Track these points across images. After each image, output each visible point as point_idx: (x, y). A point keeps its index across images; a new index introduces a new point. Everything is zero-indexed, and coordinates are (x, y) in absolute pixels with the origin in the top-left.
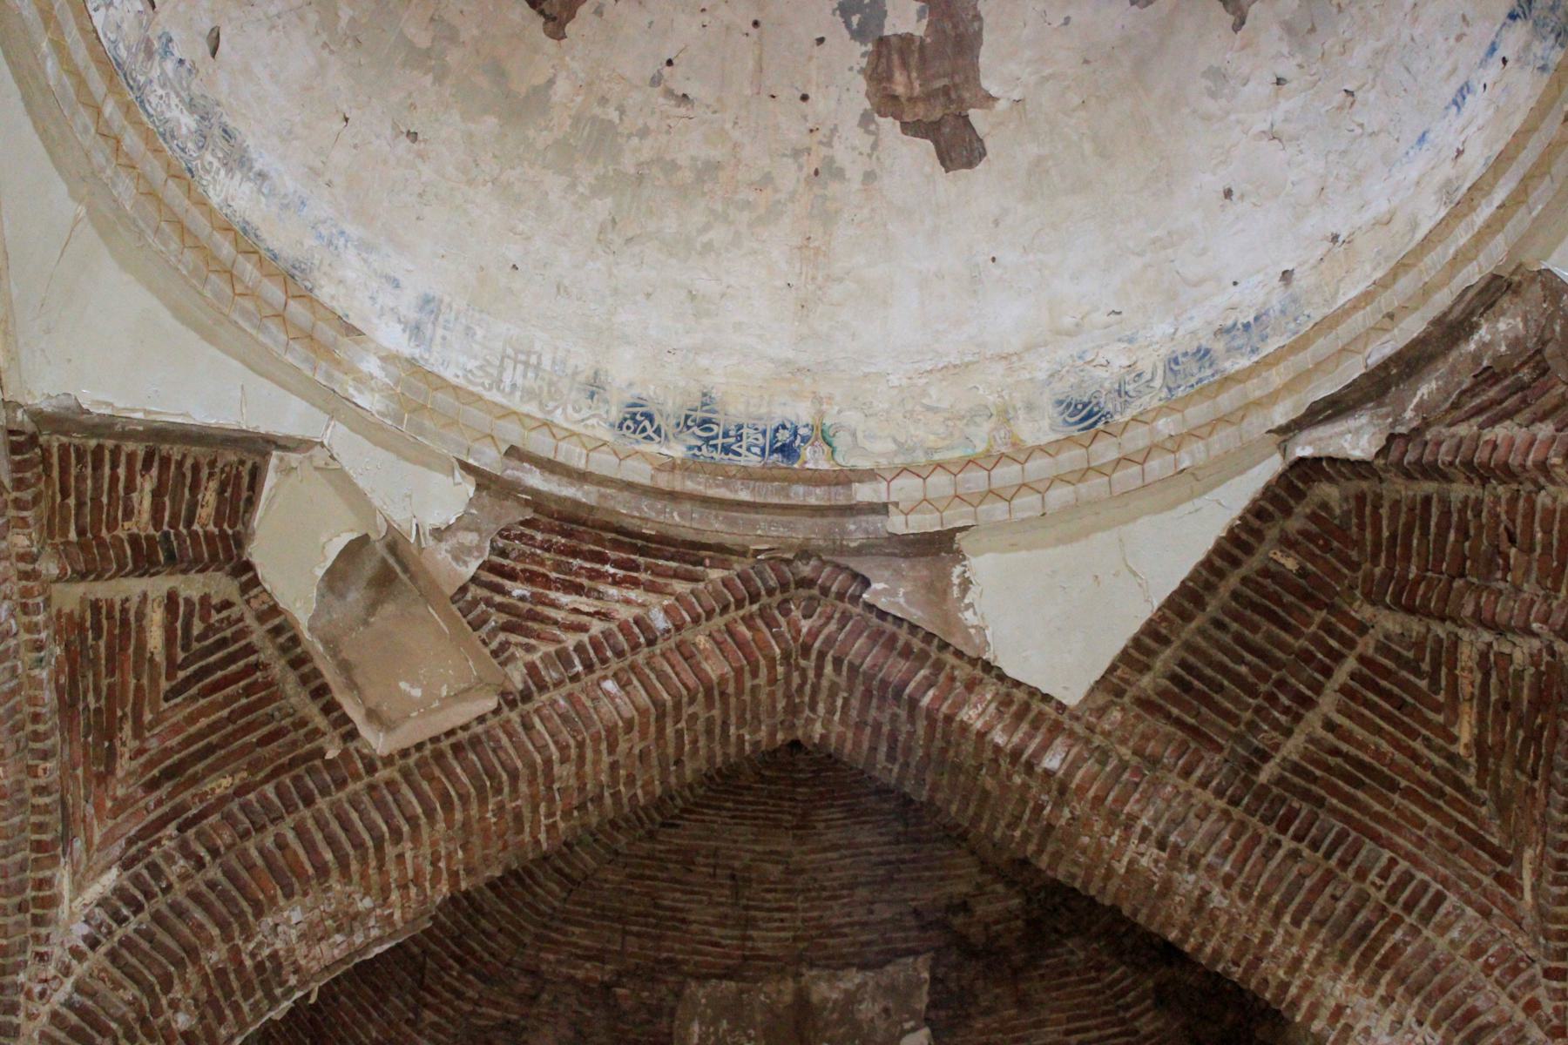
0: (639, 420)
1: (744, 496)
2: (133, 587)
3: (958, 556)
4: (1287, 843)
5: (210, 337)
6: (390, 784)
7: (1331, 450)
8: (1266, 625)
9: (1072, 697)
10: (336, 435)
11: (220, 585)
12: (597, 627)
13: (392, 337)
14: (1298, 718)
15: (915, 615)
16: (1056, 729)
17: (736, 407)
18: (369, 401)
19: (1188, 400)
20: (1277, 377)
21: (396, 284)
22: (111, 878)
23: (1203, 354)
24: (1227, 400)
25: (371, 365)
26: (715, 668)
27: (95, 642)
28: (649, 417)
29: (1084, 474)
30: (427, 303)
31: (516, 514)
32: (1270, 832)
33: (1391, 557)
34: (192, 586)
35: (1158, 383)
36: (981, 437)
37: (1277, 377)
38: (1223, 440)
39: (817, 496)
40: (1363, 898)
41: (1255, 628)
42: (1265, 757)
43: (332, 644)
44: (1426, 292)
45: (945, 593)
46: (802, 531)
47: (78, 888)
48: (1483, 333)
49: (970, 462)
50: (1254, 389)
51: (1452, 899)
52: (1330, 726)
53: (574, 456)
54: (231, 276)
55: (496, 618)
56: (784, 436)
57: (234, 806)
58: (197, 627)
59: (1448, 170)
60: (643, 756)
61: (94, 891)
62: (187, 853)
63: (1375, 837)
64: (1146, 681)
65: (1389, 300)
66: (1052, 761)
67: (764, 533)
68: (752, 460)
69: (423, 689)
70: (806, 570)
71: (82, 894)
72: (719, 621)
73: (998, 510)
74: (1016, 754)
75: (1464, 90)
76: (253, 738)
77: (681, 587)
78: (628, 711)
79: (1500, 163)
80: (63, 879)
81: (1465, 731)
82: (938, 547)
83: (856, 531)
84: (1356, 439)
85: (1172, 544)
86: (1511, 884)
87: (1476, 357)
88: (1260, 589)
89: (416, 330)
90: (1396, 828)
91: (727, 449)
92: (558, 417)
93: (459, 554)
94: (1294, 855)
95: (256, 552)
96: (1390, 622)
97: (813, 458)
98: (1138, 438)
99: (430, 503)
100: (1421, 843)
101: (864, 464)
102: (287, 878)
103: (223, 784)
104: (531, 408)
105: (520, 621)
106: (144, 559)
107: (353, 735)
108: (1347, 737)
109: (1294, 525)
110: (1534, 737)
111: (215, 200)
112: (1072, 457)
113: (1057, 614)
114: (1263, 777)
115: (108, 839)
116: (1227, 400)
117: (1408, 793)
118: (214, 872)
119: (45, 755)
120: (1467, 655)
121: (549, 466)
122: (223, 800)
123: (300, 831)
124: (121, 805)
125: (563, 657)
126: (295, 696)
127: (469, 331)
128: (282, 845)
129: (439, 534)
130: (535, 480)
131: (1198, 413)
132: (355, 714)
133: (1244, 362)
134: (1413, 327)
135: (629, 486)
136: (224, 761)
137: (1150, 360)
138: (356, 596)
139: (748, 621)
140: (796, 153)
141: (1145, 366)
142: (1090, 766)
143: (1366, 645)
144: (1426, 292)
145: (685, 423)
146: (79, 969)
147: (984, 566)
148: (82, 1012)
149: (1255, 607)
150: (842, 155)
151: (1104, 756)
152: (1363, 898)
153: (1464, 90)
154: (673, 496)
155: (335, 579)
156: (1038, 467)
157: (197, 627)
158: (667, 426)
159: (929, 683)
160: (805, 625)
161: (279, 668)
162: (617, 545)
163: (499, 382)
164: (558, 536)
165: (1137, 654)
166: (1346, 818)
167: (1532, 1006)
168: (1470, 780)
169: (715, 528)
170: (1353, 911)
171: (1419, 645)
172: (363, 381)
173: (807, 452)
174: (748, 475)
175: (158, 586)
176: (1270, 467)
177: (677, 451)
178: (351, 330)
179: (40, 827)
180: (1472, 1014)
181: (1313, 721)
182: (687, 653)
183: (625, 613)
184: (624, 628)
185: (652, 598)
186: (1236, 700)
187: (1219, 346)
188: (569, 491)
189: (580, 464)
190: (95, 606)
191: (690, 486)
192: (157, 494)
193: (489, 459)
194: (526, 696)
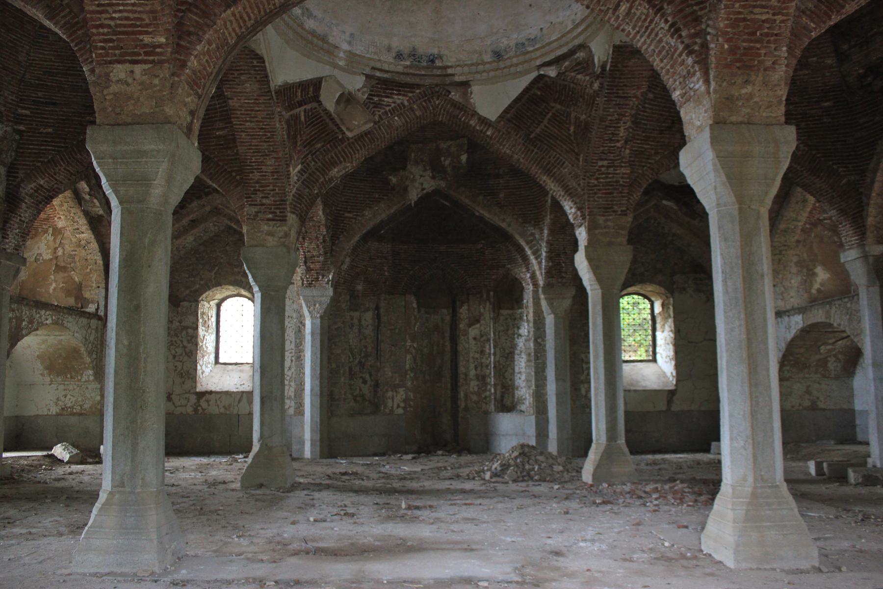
0: (399, 56)
1: (423, 73)
3: (470, 86)
4: (536, 151)
5: (308, 57)
6: (353, 143)
7: (547, 74)
9: (493, 119)
10: (337, 73)
11: (314, 105)
12: (393, 105)
13: (345, 46)
15: (461, 100)
16: (490, 125)
18: (341, 63)
19: (519, 55)
20: (538, 54)
21: (344, 32)
22: (299, 167)
23: (523, 44)
24: (527, 57)
25: (341, 55)
26: (418, 113)
27: (293, 124)
29: (497, 70)
30: (352, 35)
31: (374, 82)
32: (532, 148)
34: (308, 107)
36: (475, 58)
37: (538, 54)
38: (526, 66)
39: (439, 72)
40: (549, 162)
42: (532, 132)
43: (338, 116)
44: (567, 43)
46: (437, 81)
48: (578, 55)
49: (472, 65)
50: (533, 55)
51: (567, 163)
52: (545, 126)
53: (386, 67)
54: (312, 43)
55: (371, 106)
56: (431, 57)
59: (573, 17)
61: (296, 170)
62: (315, 161)
64: (509, 115)
65: (562, 42)
66: (489, 133)
67: (428, 81)
68: (425, 64)
69: (357, 124)
70: (437, 89)
71: (295, 171)
72: (419, 102)
73: (478, 76)
74: (481, 131)
77: (410, 95)
78: (400, 124)
79: (583, 20)
80: (291, 169)
82: (466, 85)
83: (448, 80)
84: (552, 72)
85: (517, 87)
86: (578, 160)
87: (576, 59)
89: (350, 43)
92: (382, 58)
93: (363, 94)
94: (536, 153)
95: (322, 98)
96: (559, 107)
97: (438, 63)
98: (508, 63)
99: (356, 83)
101: (450, 64)
102: (334, 164)
103: (319, 145)
104: (376, 57)
105: (377, 105)
107: (344, 133)
109: (540, 85)
111: (307, 27)
112: (494, 65)
113: (490, 101)
114: (532, 136)
115: (298, 159)
116: (527, 57)
118: (320, 164)
120: (573, 115)
121: (381, 70)
123: (336, 154)
124: (300, 150)
125: (386, 113)
127: (361, 40)
128: (332, 157)
129: (359, 90)
130: (378, 74)
131: (521, 59)
132: (344, 129)
133: (531, 49)
134: (565, 50)
135: (398, 73)
137: (512, 43)
138: (342, 105)
139: (425, 101)
141: (511, 44)
142: (496, 134)
144: (567, 43)
145: (409, 56)
146: (297, 186)
147: (475, 89)
148: (299, 195)
151: (499, 131)
152: (549, 162)
154: (408, 74)
155: (338, 102)
156: (487, 66)
158: (406, 56)
159: (463, 115)
160: (437, 102)
161: (327, 120)
162: (396, 86)
164: (383, 84)
165: (507, 111)
167: (579, 185)
168: (572, 138)
169: (417, 81)
170: (547, 164)
172: (340, 58)
173: (437, 61)
174: (424, 68)
175: (302, 108)
176: (534, 75)
177: (408, 63)
178: (337, 47)
181: (542, 125)
182: (412, 109)
183: (398, 102)
187: (526, 43)
188: (386, 76)
189: (387, 69)
191: (411, 71)
193: (368, 71)
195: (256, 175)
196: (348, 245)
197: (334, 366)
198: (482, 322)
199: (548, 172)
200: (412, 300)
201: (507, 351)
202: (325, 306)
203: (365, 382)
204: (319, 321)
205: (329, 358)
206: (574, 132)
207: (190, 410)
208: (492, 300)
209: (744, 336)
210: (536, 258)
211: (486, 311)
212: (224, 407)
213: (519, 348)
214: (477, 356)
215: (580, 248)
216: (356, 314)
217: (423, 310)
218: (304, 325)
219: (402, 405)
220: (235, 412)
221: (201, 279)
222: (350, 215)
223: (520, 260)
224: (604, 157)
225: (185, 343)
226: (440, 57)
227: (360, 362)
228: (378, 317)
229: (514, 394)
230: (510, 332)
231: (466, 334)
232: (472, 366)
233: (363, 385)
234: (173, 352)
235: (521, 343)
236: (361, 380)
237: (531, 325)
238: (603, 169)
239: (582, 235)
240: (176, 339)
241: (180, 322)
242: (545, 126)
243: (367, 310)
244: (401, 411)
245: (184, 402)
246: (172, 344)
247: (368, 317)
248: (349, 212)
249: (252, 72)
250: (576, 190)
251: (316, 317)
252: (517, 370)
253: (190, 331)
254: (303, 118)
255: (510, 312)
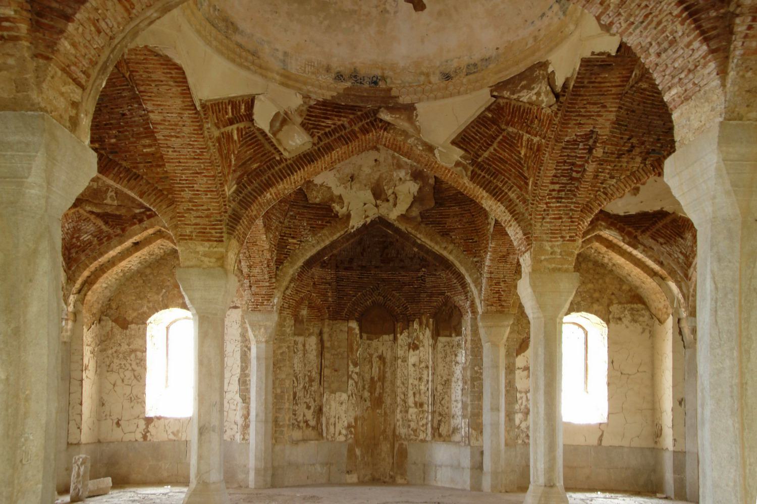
0: (339, 77)
2: (229, 128)
6: (291, 165)
8: (483, 128)
12: (333, 126)
14: (488, 148)
17: (363, 72)
28: (342, 76)
33: (512, 117)
34: (241, 125)
35: (464, 71)
41: (481, 129)
42: (480, 156)
45: (412, 118)
47: (229, 190)
52: (495, 150)
56: (375, 79)
57: (258, 170)
58: (244, 133)
60: (345, 153)
63: (501, 173)
75: (543, 15)
76: (260, 155)
77: (351, 116)
81: (523, 153)
86: (527, 184)
88: (483, 120)
90: (505, 171)
91: (361, 83)
95: (255, 117)
97: (382, 85)
100: (510, 175)
106: (231, 122)
107: (282, 154)
108: (498, 153)
110: (536, 156)
117: (509, 164)
119: (219, 166)
120: (525, 138)
122: (256, 169)
125: (325, 133)
126: (268, 146)
136: (255, 160)
140: (377, 7)
143: (505, 133)
145: (351, 77)
149: (482, 124)
150: (388, 7)
153: (543, 15)
157: (244, 133)
163: (305, 72)
166: (495, 169)
168: (522, 162)
171: (516, 134)
173: (380, 83)
175: (235, 126)
179: (220, 180)
180: (515, 211)
181: (491, 149)
183: (339, 123)
184: (339, 126)
185: (345, 119)
186: (475, 144)
190: (222, 133)
192: (232, 109)
194: (318, 143)
195: (187, 194)
196: (291, 270)
197: (279, 391)
198: (421, 349)
199: (497, 194)
200: (354, 325)
201: (445, 378)
202: (269, 331)
203: (308, 407)
204: (263, 345)
205: (274, 383)
206: (525, 155)
207: (139, 436)
208: (431, 327)
209: (736, 381)
210: (476, 286)
211: (426, 336)
212: (173, 433)
213: (455, 375)
214: (416, 382)
215: (523, 275)
216: (300, 339)
217: (365, 336)
218: (249, 349)
219: (344, 432)
220: (184, 439)
221: (149, 302)
222: (295, 241)
223: (459, 287)
224: (556, 180)
225: (134, 366)
226: (384, 78)
227: (304, 387)
228: (322, 341)
229: (449, 423)
230: (448, 359)
231: (405, 360)
232: (411, 393)
233: (306, 411)
234: (122, 376)
235: (458, 371)
236: (305, 405)
237: (468, 352)
238: (554, 193)
239: (526, 261)
240: (125, 362)
241: (129, 345)
242: (495, 150)
243: (310, 335)
244: (342, 438)
245: (133, 428)
246: (121, 368)
247: (313, 341)
248: (293, 238)
249: (172, 83)
250: (523, 215)
251: (261, 342)
252: (453, 398)
253: (139, 353)
254: (236, 137)
255: (448, 339)
